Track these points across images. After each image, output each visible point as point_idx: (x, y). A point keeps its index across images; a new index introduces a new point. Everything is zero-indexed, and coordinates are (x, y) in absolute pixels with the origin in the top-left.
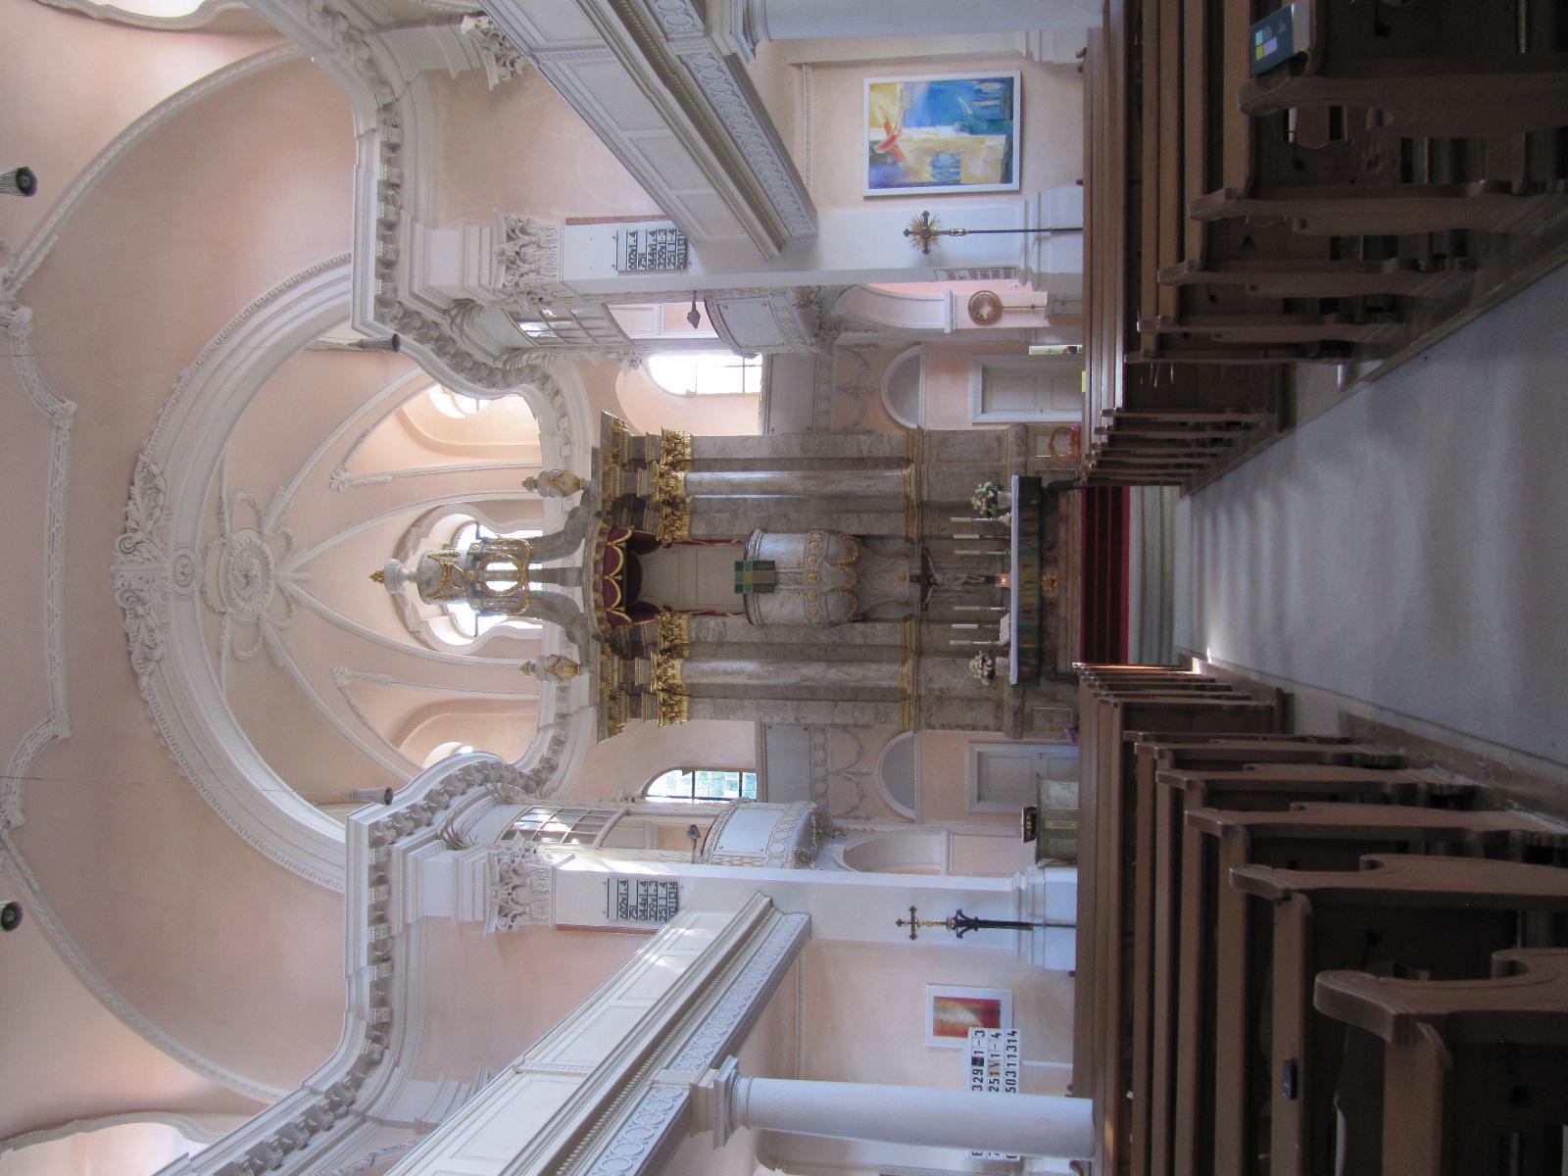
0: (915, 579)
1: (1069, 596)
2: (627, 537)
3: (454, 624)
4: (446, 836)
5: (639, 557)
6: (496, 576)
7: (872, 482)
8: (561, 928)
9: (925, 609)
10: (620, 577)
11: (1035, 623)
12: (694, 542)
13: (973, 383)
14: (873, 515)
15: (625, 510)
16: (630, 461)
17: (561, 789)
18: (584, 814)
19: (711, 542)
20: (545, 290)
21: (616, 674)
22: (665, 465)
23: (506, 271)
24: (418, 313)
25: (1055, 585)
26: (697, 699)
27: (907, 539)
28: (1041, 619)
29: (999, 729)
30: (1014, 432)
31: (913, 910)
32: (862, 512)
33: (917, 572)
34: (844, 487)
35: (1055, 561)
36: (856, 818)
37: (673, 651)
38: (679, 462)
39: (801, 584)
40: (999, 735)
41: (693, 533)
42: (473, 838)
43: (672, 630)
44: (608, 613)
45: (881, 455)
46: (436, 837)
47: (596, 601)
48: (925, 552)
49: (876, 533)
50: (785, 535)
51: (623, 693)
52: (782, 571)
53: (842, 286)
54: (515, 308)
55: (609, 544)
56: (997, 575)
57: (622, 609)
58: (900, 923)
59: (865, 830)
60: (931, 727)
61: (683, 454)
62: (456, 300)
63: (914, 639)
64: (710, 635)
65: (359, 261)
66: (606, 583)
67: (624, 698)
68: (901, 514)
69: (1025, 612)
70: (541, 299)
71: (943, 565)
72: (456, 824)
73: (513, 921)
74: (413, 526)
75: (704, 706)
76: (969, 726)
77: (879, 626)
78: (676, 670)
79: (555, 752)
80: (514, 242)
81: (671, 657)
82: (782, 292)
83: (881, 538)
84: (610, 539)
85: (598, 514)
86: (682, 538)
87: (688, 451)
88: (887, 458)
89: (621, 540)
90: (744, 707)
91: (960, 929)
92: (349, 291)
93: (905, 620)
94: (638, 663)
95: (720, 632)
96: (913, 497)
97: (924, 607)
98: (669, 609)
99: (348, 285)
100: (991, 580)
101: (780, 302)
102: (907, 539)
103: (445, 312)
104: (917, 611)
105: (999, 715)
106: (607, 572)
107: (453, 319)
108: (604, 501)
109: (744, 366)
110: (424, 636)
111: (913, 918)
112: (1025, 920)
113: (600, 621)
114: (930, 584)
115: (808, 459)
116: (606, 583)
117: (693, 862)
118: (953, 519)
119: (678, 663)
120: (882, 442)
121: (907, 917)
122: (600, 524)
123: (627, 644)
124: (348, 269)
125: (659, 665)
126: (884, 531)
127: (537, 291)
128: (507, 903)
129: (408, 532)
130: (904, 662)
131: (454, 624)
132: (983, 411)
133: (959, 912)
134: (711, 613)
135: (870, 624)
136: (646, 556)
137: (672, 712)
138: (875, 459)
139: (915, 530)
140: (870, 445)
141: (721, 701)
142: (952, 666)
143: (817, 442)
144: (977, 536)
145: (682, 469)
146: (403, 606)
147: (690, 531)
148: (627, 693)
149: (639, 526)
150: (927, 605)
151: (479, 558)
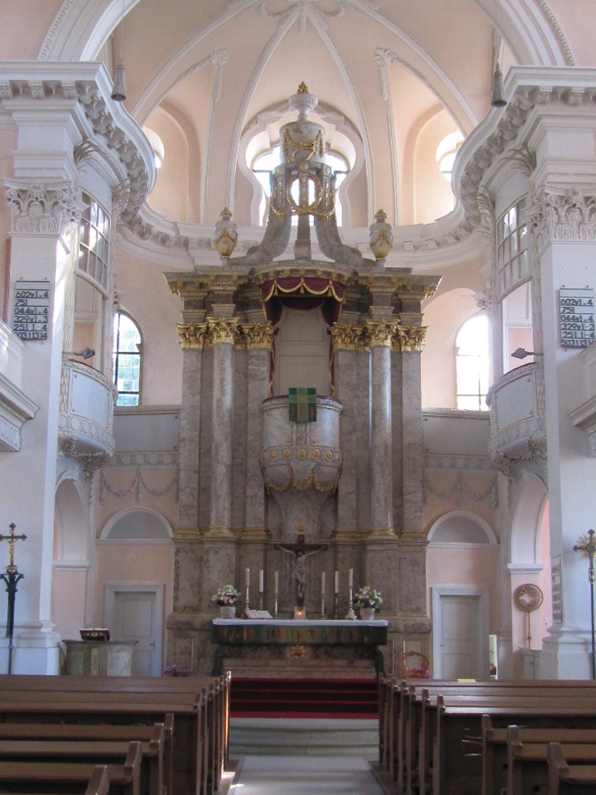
0: (301, 539)
1: (287, 669)
2: (336, 297)
3: (263, 152)
4: (86, 145)
5: (319, 307)
6: (304, 195)
7: (382, 503)
8: (8, 242)
9: (276, 547)
10: (302, 291)
11: (264, 640)
12: (332, 354)
13: (466, 588)
14: (354, 504)
15: (359, 296)
16: (400, 300)
17: (124, 242)
18: (104, 262)
19: (332, 368)
20: (543, 229)
21: (221, 288)
22: (397, 330)
23: (559, 196)
24: (524, 122)
25: (297, 657)
26: (200, 357)
27: (335, 533)
28: (268, 645)
29: (175, 609)
30: (424, 622)
31: (24, 537)
32: (357, 495)
33: (307, 541)
34: (378, 479)
35: (317, 657)
36: (101, 490)
37: (241, 336)
38: (399, 341)
39: (297, 444)
40: (170, 610)
41: (340, 354)
42: (83, 168)
43: (258, 335)
44: (272, 282)
45: (405, 511)
46: (85, 138)
47: (282, 271)
48: (324, 547)
49: (340, 506)
50: (338, 430)
51: (206, 294)
52: (308, 428)
53: (547, 478)
54: (529, 203)
55: (331, 283)
56: (305, 608)
57: (276, 293)
58: (13, 526)
59: (91, 497)
60: (177, 553)
61: (406, 344)
62: (535, 154)
63: (251, 538)
64: (255, 367)
65: (568, 73)
66: (298, 280)
67: (202, 295)
68: (356, 527)
69: (273, 631)
70: (536, 225)
71: (313, 562)
72: (95, 154)
73: (14, 201)
74: (346, 118)
75: (195, 362)
76: (178, 584)
77: (262, 509)
78: (225, 339)
79: (156, 237)
80: (584, 202)
81: (236, 335)
82: (542, 427)
83: (336, 511)
84: (334, 283)
85: (355, 273)
86: (335, 343)
87: (409, 349)
88: (402, 516)
89: (334, 292)
90: (194, 396)
91: (7, 577)
92: (542, 64)
93: (267, 531)
94: (231, 307)
95: (256, 376)
96: (370, 538)
97: (278, 546)
98: (276, 332)
99: (548, 63)
100: (300, 603)
101: (533, 426)
102: (335, 533)
103: (525, 145)
104: (275, 540)
105: (187, 609)
106: (307, 280)
107: (519, 151)
108: (366, 278)
109: (480, 395)
110: (254, 127)
111: (17, 537)
112: (15, 630)
113: (266, 275)
114: (297, 552)
115: (402, 449)
116: (298, 280)
117: (63, 353)
118: (351, 571)
119: (231, 340)
120: (416, 511)
121: (17, 532)
122: (347, 275)
123: (246, 298)
124: (561, 64)
125: (229, 324)
126: (341, 513)
127: (543, 223)
128: (30, 196)
129: (340, 113)
130: (232, 530)
131: (263, 152)
132: (442, 596)
133: (21, 576)
134: (272, 368)
135: (263, 501)
136: (320, 313)
137: (189, 335)
138: (402, 506)
139: (342, 539)
140: (413, 502)
141: (199, 376)
142: (229, 570)
143: (416, 457)
144: (337, 591)
145: (393, 344)
146: (278, 109)
147: (341, 350)
148: (205, 297)
149: (345, 307)
150: (279, 549)
151: (318, 173)
